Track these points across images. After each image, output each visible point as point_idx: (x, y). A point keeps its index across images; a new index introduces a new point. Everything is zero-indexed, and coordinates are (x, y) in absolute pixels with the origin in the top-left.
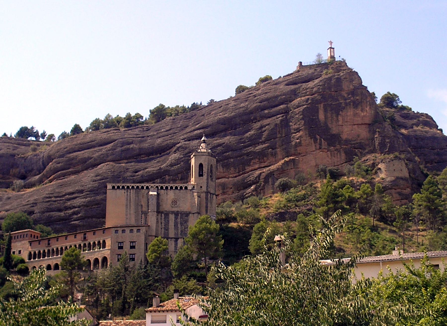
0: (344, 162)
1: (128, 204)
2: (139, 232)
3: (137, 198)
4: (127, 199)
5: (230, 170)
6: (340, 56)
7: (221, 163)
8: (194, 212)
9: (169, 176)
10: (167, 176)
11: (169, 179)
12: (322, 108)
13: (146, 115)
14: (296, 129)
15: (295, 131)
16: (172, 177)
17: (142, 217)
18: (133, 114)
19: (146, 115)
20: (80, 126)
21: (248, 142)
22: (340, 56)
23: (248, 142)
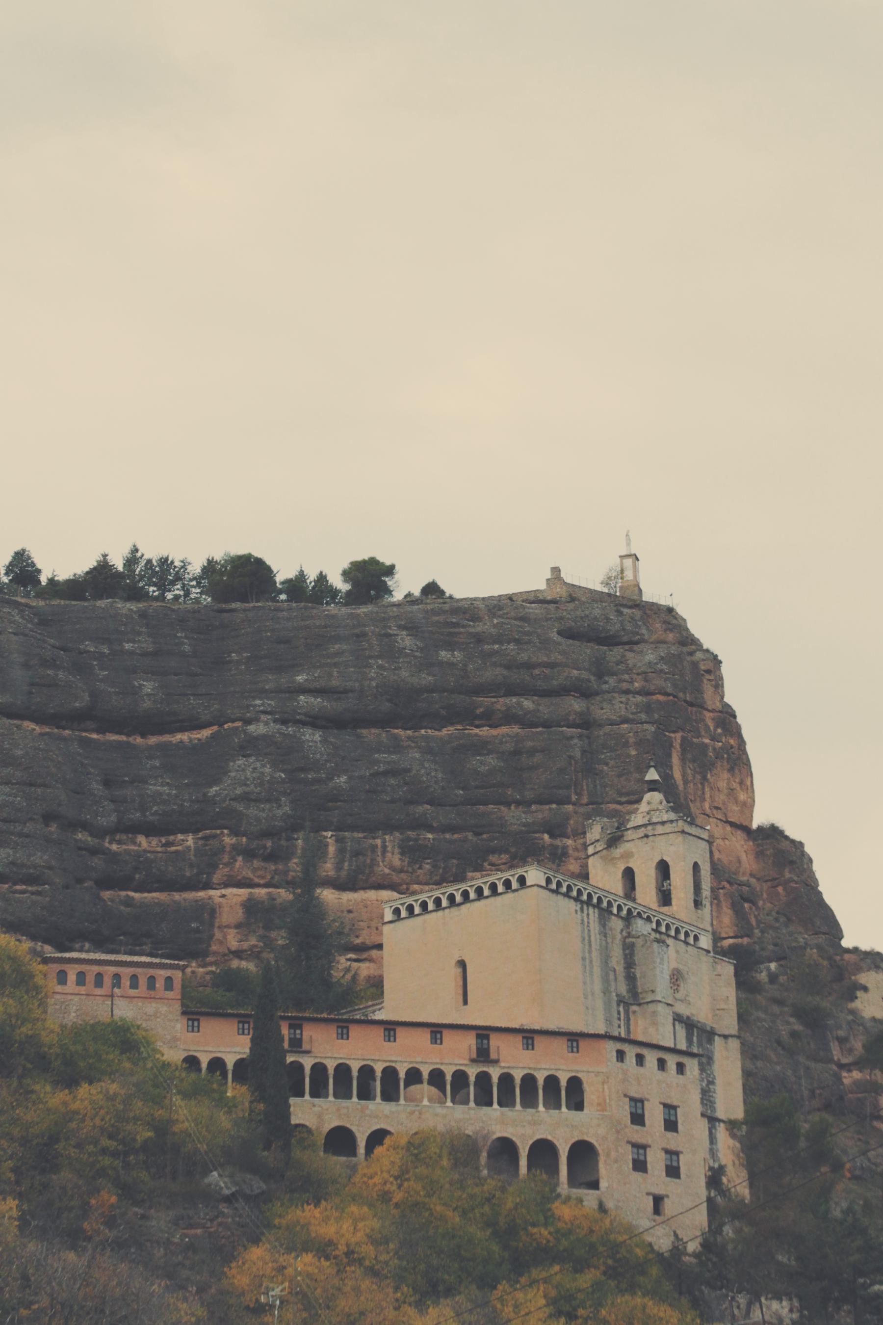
0: (731, 934)
1: (587, 955)
2: (198, 1031)
3: (604, 943)
4: (584, 939)
5: (420, 868)
6: (671, 595)
7: (397, 834)
8: (727, 1033)
9: (235, 833)
10: (226, 831)
11: (234, 847)
12: (678, 747)
13: (447, 595)
14: (628, 794)
15: (624, 799)
16: (244, 839)
17: (619, 1013)
18: (218, 558)
19: (447, 595)
20: (378, 558)
21: (477, 787)
22: (671, 595)
23: (477, 787)
